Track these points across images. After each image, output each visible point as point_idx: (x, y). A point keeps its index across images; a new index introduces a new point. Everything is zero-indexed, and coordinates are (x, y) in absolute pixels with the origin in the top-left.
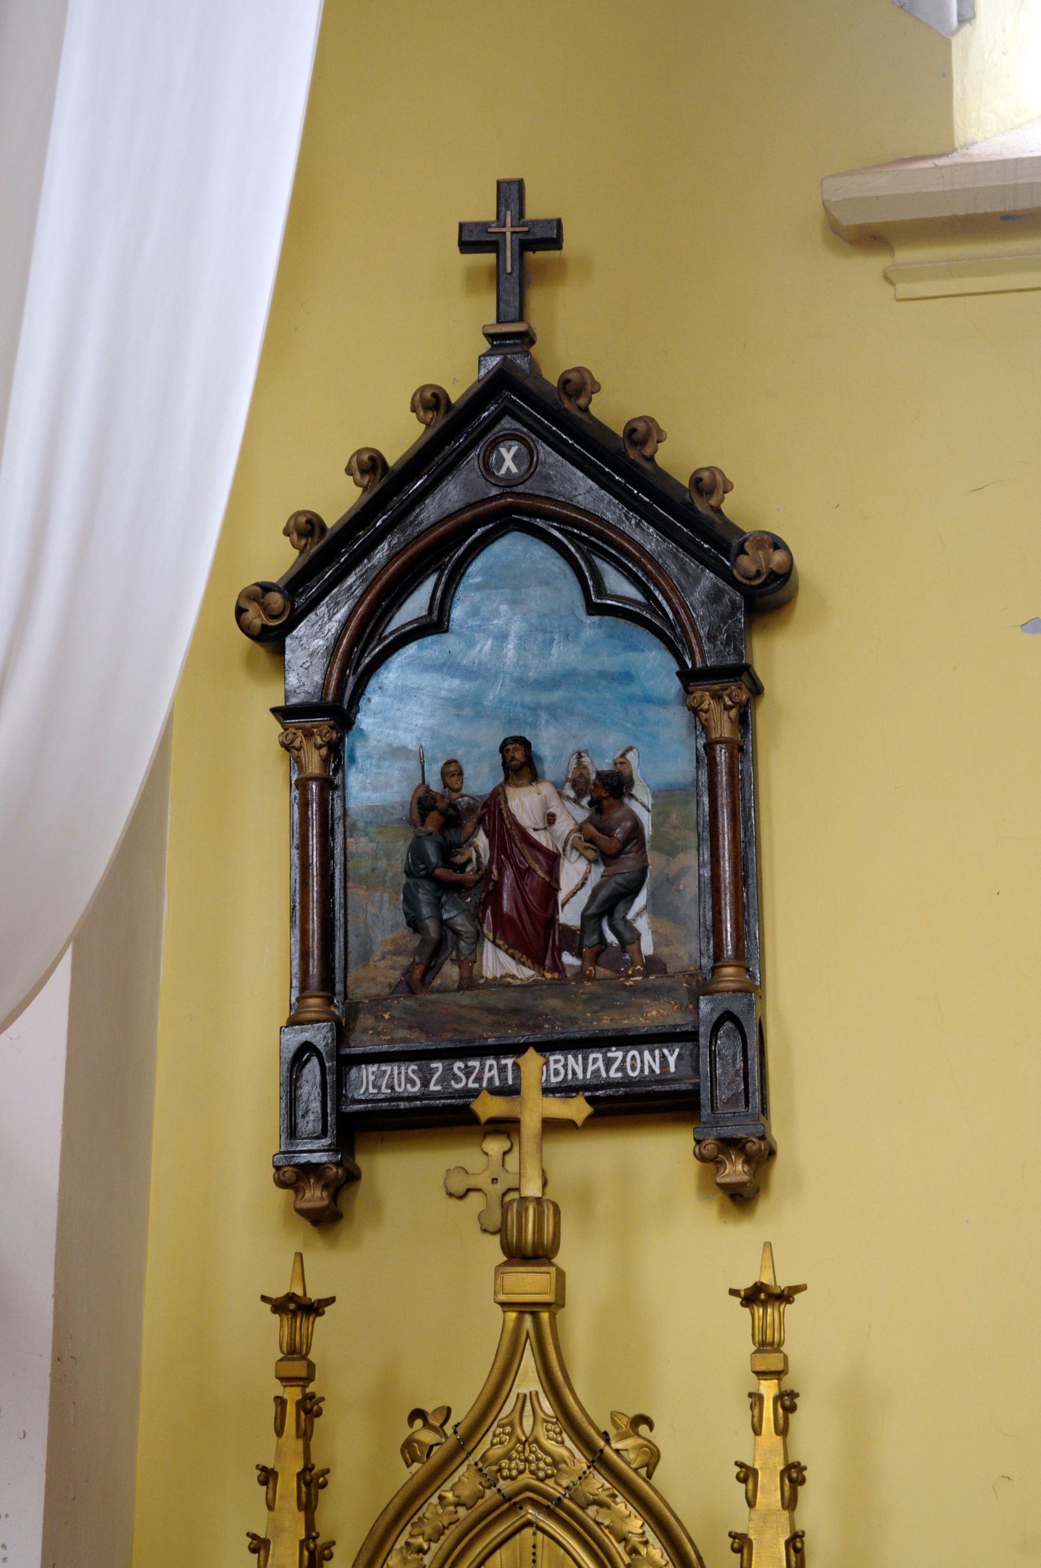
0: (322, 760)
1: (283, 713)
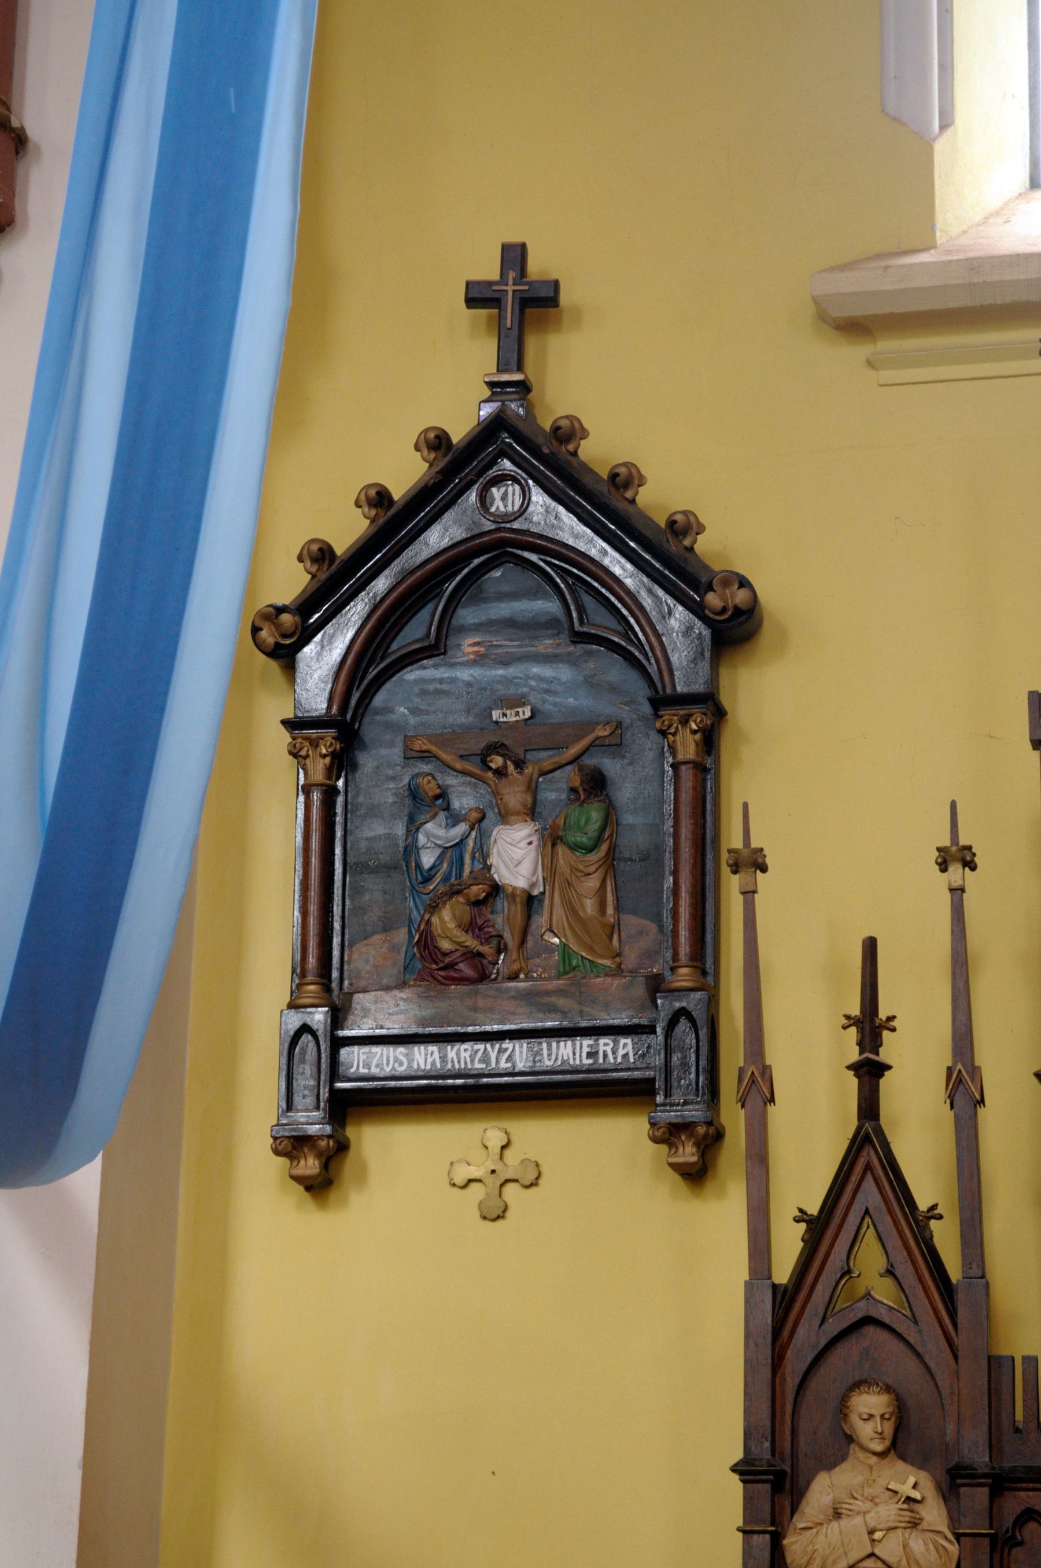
0: (326, 769)
1: (293, 725)
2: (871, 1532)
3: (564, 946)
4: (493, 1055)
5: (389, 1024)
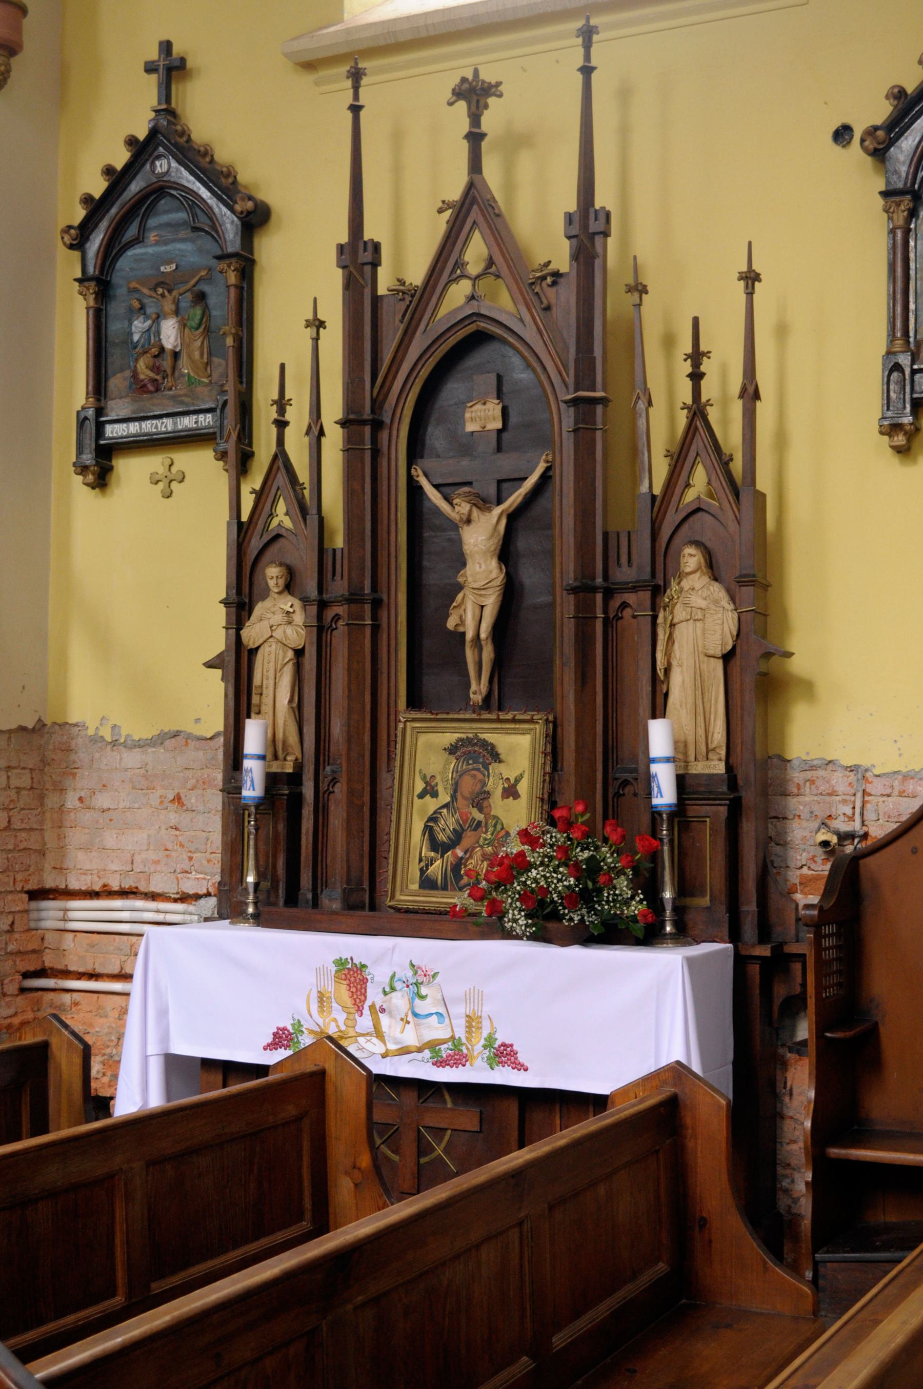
2: (271, 627)
3: (189, 373)
4: (159, 425)
5: (121, 414)
